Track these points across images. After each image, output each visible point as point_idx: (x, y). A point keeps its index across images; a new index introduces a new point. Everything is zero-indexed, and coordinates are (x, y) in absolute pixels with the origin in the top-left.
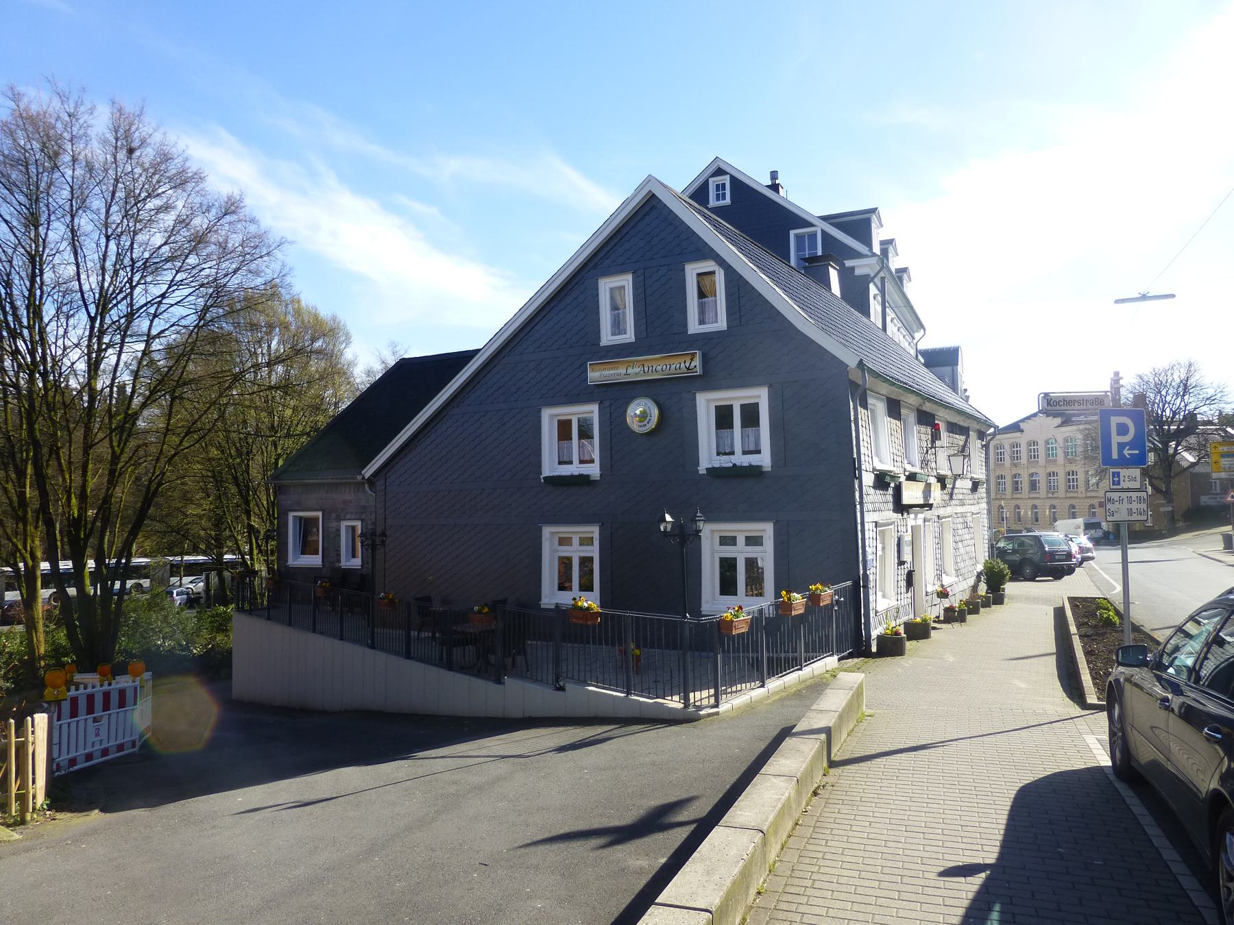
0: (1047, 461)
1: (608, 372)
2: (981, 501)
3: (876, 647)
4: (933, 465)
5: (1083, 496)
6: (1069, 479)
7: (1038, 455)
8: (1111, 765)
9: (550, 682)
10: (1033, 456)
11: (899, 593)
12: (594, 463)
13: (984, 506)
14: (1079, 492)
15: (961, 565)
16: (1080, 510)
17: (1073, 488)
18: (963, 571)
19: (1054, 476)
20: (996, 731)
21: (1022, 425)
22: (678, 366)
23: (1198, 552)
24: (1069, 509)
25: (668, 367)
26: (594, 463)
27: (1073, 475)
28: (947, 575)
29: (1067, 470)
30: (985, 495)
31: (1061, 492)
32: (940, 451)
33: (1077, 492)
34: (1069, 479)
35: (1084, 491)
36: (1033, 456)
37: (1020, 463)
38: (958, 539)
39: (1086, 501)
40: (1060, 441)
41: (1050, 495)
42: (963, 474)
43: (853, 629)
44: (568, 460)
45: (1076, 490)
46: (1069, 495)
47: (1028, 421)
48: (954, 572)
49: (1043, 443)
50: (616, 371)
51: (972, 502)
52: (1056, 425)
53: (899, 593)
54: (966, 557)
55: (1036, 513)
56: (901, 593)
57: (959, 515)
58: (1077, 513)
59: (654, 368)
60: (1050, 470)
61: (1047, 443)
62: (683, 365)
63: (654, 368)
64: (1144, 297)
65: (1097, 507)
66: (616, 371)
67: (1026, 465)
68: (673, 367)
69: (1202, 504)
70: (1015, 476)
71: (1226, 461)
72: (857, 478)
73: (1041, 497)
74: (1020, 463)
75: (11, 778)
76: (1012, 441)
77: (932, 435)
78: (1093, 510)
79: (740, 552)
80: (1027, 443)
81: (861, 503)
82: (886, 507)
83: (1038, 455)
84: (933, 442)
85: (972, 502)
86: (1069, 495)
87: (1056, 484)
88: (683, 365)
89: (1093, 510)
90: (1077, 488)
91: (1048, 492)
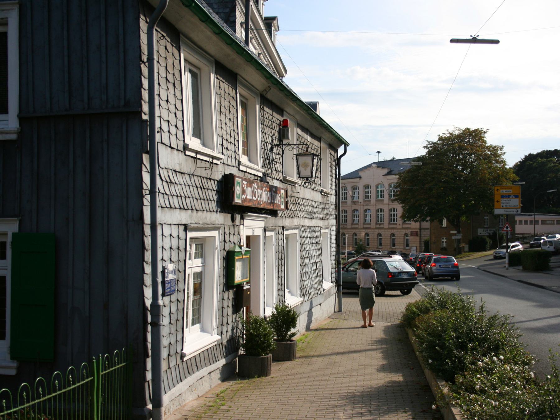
0: (377, 201)
2: (330, 216)
4: (279, 167)
5: (401, 227)
6: (391, 214)
7: (370, 196)
10: (367, 196)
11: (225, 323)
13: (333, 222)
14: (398, 224)
15: (308, 283)
16: (398, 238)
17: (394, 221)
18: (309, 290)
19: (381, 212)
21: (361, 174)
23: (483, 269)
24: (391, 237)
27: (394, 211)
28: (292, 295)
29: (390, 208)
30: (333, 211)
31: (386, 225)
32: (287, 149)
33: (396, 224)
34: (391, 214)
35: (401, 224)
36: (367, 196)
37: (358, 201)
38: (305, 254)
39: (402, 230)
40: (386, 185)
41: (378, 226)
42: (312, 177)
45: (395, 222)
46: (391, 226)
47: (365, 170)
48: (299, 291)
49: (375, 186)
51: (321, 216)
52: (384, 174)
53: (225, 323)
54: (313, 274)
55: (368, 239)
56: (227, 323)
57: (307, 229)
58: (396, 240)
60: (378, 207)
61: (377, 186)
64: (474, 40)
65: (410, 236)
67: (362, 204)
69: (479, 234)
70: (354, 211)
71: (504, 201)
72: (147, 152)
73: (372, 227)
74: (358, 201)
76: (353, 184)
77: (279, 133)
78: (407, 238)
80: (364, 186)
81: (153, 192)
82: (205, 205)
83: (370, 196)
84: (281, 140)
85: (321, 216)
86: (391, 226)
87: (382, 218)
89: (407, 238)
90: (397, 221)
91: (376, 224)
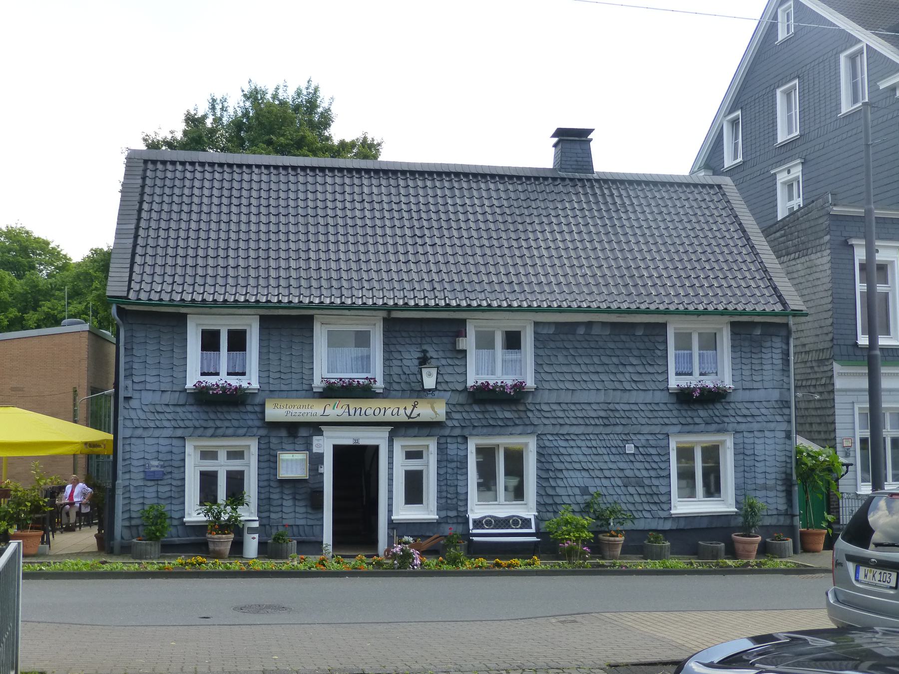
1: (298, 411)
3: (350, 442)
8: (865, 258)
9: (829, 367)
12: (219, 375)
20: (231, 623)
22: (395, 411)
25: (383, 411)
26: (219, 375)
43: (422, 513)
44: (241, 371)
50: (309, 411)
59: (363, 412)
62: (402, 411)
63: (363, 412)
66: (309, 411)
68: (389, 412)
75: (890, 368)
79: (222, 467)
88: (402, 411)
